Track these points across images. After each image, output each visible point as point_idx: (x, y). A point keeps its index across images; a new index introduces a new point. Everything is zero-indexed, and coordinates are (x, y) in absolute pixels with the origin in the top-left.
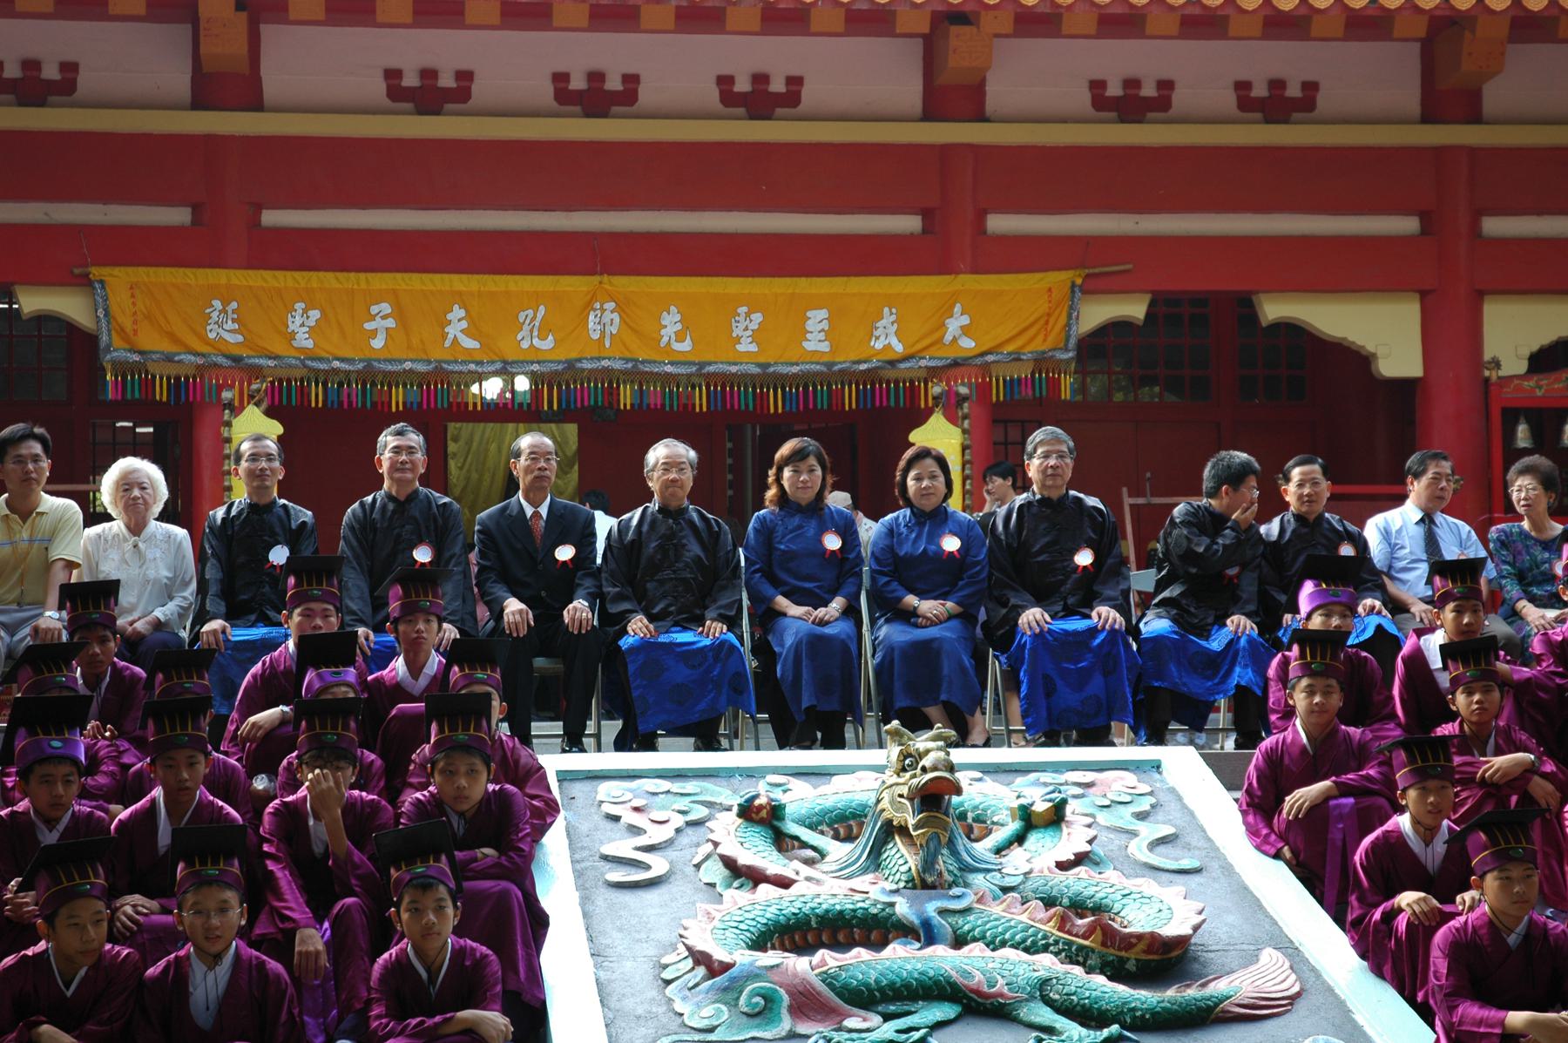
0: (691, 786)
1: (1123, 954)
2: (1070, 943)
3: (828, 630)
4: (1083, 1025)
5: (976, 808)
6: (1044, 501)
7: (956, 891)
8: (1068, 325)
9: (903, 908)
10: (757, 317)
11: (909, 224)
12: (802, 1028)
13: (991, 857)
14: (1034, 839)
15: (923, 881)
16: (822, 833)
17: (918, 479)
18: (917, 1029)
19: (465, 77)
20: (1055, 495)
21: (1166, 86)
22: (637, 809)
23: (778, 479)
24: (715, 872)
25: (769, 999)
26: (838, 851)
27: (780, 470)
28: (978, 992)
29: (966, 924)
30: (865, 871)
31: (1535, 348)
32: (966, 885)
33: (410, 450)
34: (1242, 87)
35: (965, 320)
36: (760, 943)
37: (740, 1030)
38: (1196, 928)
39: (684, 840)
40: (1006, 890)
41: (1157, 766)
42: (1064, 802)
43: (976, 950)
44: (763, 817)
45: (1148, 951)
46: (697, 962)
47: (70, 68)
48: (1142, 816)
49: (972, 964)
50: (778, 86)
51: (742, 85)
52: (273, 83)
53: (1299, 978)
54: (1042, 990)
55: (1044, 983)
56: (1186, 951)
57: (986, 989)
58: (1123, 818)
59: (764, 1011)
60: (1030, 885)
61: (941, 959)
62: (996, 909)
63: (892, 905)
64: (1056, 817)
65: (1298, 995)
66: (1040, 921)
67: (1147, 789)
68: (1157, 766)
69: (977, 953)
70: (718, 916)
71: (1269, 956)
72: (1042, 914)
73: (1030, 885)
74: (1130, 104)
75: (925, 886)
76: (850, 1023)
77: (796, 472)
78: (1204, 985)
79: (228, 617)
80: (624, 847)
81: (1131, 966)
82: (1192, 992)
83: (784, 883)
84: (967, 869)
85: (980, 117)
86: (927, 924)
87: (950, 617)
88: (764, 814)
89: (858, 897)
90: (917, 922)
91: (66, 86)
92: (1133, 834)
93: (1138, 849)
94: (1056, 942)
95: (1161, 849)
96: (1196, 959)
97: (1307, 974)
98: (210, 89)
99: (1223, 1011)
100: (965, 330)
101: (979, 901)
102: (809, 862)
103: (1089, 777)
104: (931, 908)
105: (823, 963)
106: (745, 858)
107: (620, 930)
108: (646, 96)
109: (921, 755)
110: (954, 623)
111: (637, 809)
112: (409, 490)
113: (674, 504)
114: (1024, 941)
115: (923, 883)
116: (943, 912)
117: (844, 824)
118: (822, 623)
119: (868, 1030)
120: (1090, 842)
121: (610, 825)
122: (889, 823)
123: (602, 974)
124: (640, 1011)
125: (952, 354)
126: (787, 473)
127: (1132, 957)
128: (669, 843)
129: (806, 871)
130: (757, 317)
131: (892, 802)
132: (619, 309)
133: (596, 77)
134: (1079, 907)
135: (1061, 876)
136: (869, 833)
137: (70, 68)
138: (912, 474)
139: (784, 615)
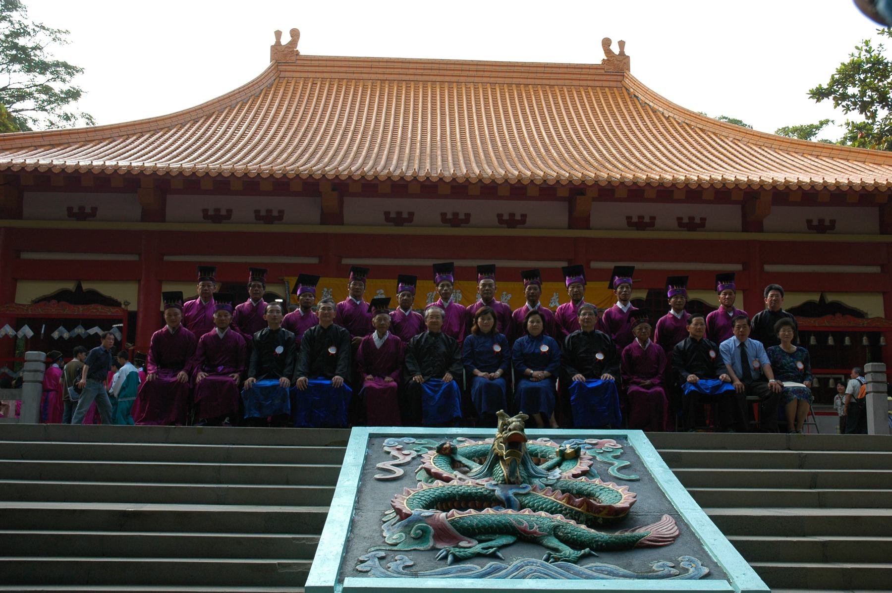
0: (423, 441)
1: (596, 515)
2: (571, 510)
3: (495, 382)
4: (572, 548)
5: (542, 451)
6: (584, 333)
7: (524, 485)
9: (498, 492)
10: (510, 296)
12: (438, 546)
13: (545, 472)
14: (565, 465)
15: (509, 480)
16: (474, 461)
17: (532, 322)
18: (492, 548)
20: (589, 330)
22: (398, 449)
23: (476, 322)
24: (423, 475)
25: (424, 531)
26: (476, 468)
27: (477, 319)
28: (525, 531)
29: (526, 500)
30: (485, 476)
32: (530, 483)
33: (329, 309)
34: (680, 219)
36: (427, 507)
37: (409, 545)
38: (632, 504)
39: (415, 462)
40: (547, 485)
41: (626, 437)
42: (579, 449)
43: (527, 511)
44: (448, 454)
45: (608, 514)
46: (397, 514)
48: (616, 457)
49: (524, 517)
53: (679, 528)
54: (555, 531)
55: (556, 527)
56: (628, 514)
57: (528, 529)
58: (609, 458)
59: (421, 537)
60: (559, 484)
61: (509, 515)
62: (541, 494)
63: (494, 491)
64: (576, 456)
65: (678, 536)
66: (560, 500)
67: (620, 446)
68: (626, 437)
69: (527, 513)
70: (413, 493)
71: (666, 518)
72: (560, 496)
73: (559, 484)
74: (640, 224)
75: (510, 483)
76: (462, 544)
77: (483, 319)
78: (633, 531)
79: (256, 377)
80: (387, 465)
81: (600, 521)
82: (627, 534)
83: (447, 480)
84: (531, 476)
85: (588, 228)
86: (508, 499)
87: (546, 378)
88: (447, 451)
89: (480, 487)
90: (503, 498)
91: (280, 217)
92: (612, 464)
94: (566, 509)
95: (623, 471)
96: (632, 519)
97: (683, 526)
98: (325, 219)
99: (641, 543)
101: (534, 490)
102: (465, 473)
103: (594, 441)
104: (511, 493)
105: (453, 515)
106: (435, 469)
107: (373, 499)
109: (510, 423)
110: (547, 381)
111: (398, 449)
112: (329, 324)
113: (435, 331)
114: (551, 508)
115: (508, 482)
116: (516, 495)
117: (479, 456)
118: (492, 379)
119: (470, 547)
120: (590, 466)
121: (385, 455)
122: (497, 455)
123: (356, 518)
124: (367, 535)
126: (479, 320)
127: (601, 516)
128: (408, 463)
129: (460, 475)
130: (510, 296)
131: (498, 445)
132: (462, 292)
134: (580, 493)
135: (574, 480)
136: (489, 459)
138: (530, 319)
139: (477, 376)
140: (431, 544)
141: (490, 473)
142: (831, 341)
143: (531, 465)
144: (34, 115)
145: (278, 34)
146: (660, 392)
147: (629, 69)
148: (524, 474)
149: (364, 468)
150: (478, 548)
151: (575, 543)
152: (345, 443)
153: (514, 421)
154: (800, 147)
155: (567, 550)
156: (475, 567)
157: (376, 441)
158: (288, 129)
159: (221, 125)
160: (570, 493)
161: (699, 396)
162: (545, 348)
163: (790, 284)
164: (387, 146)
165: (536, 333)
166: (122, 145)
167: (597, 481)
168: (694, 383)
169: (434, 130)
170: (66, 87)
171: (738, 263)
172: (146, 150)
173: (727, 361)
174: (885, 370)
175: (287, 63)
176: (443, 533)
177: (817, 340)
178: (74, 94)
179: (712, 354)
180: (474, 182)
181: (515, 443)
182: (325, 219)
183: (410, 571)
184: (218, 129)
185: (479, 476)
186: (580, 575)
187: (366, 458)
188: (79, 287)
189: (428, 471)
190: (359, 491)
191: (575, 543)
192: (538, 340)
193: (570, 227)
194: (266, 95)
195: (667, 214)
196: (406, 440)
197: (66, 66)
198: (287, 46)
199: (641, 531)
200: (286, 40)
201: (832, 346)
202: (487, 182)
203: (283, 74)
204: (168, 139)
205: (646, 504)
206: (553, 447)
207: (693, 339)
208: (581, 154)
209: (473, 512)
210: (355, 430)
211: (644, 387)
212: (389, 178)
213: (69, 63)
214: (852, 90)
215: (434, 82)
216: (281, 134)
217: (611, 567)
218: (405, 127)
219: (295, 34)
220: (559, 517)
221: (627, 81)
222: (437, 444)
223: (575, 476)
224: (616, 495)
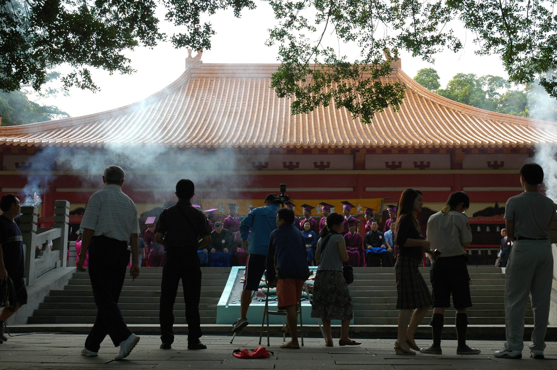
8: (381, 209)
11: (351, 189)
19: (329, 163)
21: (400, 163)
31: (474, 212)
34: (415, 163)
35: (361, 207)
47: (329, 163)
50: (325, 164)
51: (319, 164)
100: (361, 209)
108: (331, 166)
125: (358, 214)
133: (496, 162)
137: (329, 163)
140: (256, 297)
142: (488, 229)
146: (357, 253)
147: (400, 67)
149: (236, 279)
152: (229, 273)
154: (494, 116)
157: (241, 271)
158: (198, 112)
161: (372, 254)
162: (310, 236)
164: (254, 122)
165: (307, 229)
168: (370, 249)
171: (448, 187)
173: (387, 240)
177: (481, 229)
179: (381, 237)
180: (298, 148)
187: (237, 276)
188: (496, 205)
190: (234, 286)
192: (308, 232)
193: (354, 169)
195: (408, 161)
198: (195, 58)
201: (479, 232)
202: (305, 148)
207: (373, 231)
210: (233, 267)
211: (351, 251)
216: (193, 116)
218: (265, 109)
221: (399, 74)
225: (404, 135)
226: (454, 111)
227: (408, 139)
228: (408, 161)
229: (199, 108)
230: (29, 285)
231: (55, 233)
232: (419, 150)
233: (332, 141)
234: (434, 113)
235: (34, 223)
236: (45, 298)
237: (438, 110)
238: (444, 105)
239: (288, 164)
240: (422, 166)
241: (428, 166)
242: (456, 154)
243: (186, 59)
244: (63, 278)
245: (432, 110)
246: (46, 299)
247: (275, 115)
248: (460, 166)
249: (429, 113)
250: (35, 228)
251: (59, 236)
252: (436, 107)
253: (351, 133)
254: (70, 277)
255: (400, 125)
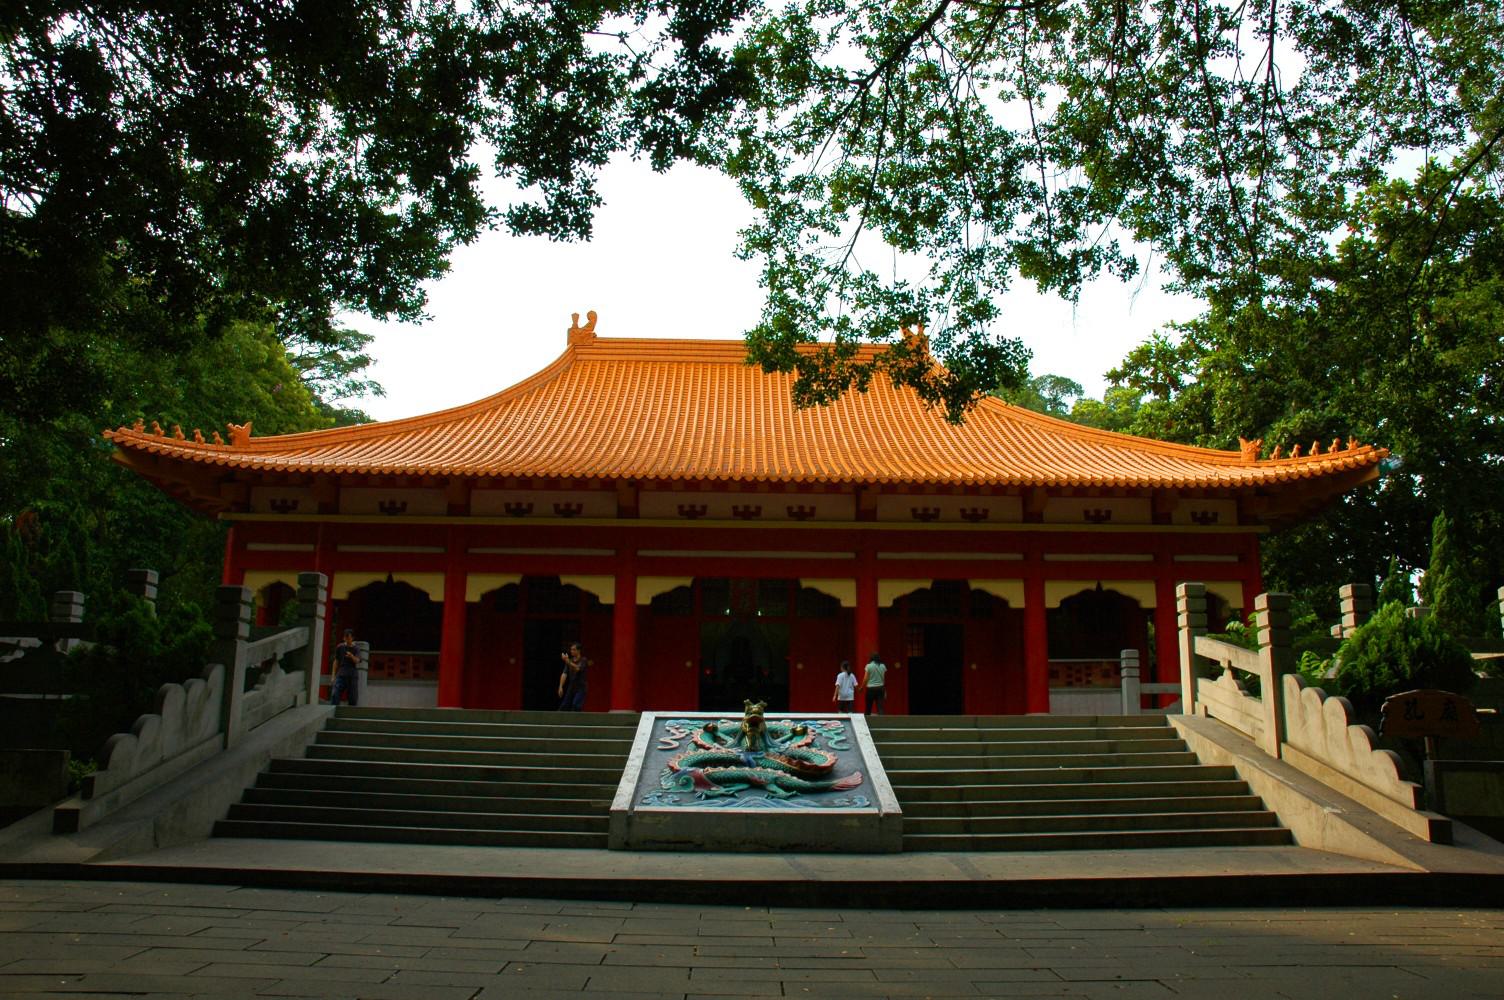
0: (695, 722)
9: (742, 757)
25: (688, 780)
26: (730, 740)
36: (692, 766)
38: (832, 765)
43: (758, 769)
44: (711, 731)
48: (837, 734)
49: (756, 772)
52: (643, 509)
54: (776, 781)
55: (776, 779)
59: (686, 784)
64: (804, 732)
68: (849, 720)
80: (667, 739)
83: (708, 749)
93: (831, 744)
102: (722, 745)
103: (824, 722)
104: (751, 757)
106: (701, 741)
115: (752, 749)
117: (732, 733)
137: (704, 508)
140: (692, 788)
141: (739, 744)
143: (769, 739)
144: (322, 383)
145: (575, 317)
148: (762, 745)
150: (722, 790)
151: (787, 788)
153: (755, 707)
155: (781, 792)
156: (719, 801)
157: (660, 723)
158: (586, 417)
159: (519, 413)
160: (791, 758)
163: (1067, 572)
166: (427, 438)
167: (813, 750)
169: (729, 417)
170: (353, 355)
172: (451, 443)
174: (1137, 655)
175: (583, 346)
176: (700, 782)
178: (363, 362)
181: (755, 722)
182: (623, 513)
183: (676, 803)
184: (516, 419)
185: (731, 746)
186: (786, 806)
188: (390, 578)
189: (696, 743)
191: (787, 788)
194: (563, 380)
196: (682, 721)
197: (356, 334)
198: (584, 329)
199: (835, 782)
200: (583, 322)
203: (579, 357)
204: (469, 430)
205: (845, 763)
206: (787, 725)
208: (871, 443)
209: (722, 769)
212: (682, 477)
213: (360, 332)
214: (1145, 373)
215: (731, 364)
217: (807, 801)
219: (592, 317)
220: (780, 772)
222: (703, 724)
223: (799, 746)
224: (822, 758)
225: (942, 462)
226: (1020, 423)
227: (905, 469)
228: (950, 506)
229: (588, 411)
230: (229, 746)
231: (291, 638)
232: (972, 489)
233: (820, 470)
234: (988, 427)
235: (320, 617)
236: (260, 776)
237: (994, 423)
238: (1003, 412)
239: (686, 509)
240: (975, 516)
241: (402, 509)
242: (1030, 495)
243: (569, 330)
244: (303, 731)
245: (985, 422)
246: (261, 779)
247: (718, 426)
248: (634, 513)
249: (979, 427)
250: (244, 630)
251: (302, 642)
252: (990, 417)
253: (851, 457)
254: (320, 727)
255: (934, 445)
